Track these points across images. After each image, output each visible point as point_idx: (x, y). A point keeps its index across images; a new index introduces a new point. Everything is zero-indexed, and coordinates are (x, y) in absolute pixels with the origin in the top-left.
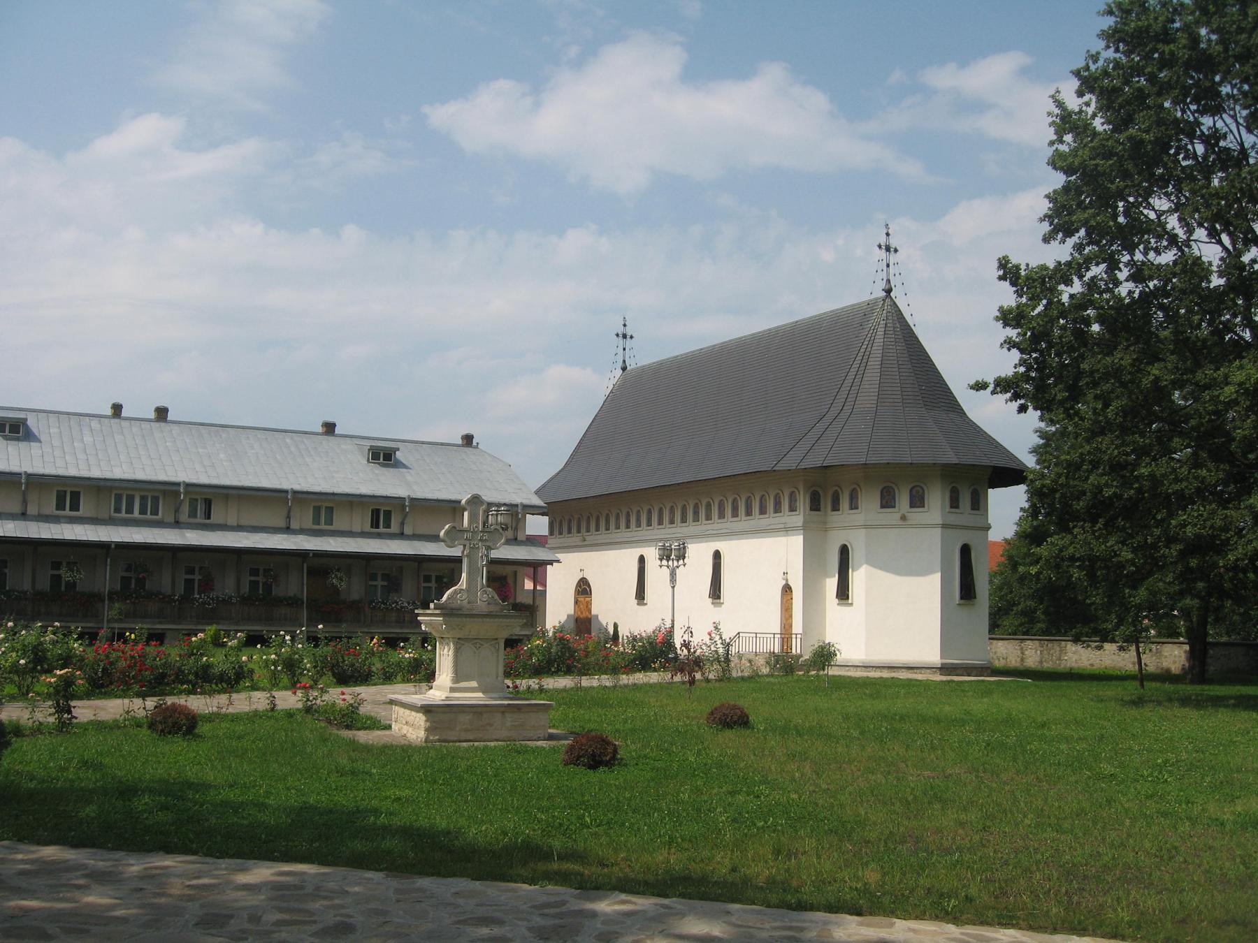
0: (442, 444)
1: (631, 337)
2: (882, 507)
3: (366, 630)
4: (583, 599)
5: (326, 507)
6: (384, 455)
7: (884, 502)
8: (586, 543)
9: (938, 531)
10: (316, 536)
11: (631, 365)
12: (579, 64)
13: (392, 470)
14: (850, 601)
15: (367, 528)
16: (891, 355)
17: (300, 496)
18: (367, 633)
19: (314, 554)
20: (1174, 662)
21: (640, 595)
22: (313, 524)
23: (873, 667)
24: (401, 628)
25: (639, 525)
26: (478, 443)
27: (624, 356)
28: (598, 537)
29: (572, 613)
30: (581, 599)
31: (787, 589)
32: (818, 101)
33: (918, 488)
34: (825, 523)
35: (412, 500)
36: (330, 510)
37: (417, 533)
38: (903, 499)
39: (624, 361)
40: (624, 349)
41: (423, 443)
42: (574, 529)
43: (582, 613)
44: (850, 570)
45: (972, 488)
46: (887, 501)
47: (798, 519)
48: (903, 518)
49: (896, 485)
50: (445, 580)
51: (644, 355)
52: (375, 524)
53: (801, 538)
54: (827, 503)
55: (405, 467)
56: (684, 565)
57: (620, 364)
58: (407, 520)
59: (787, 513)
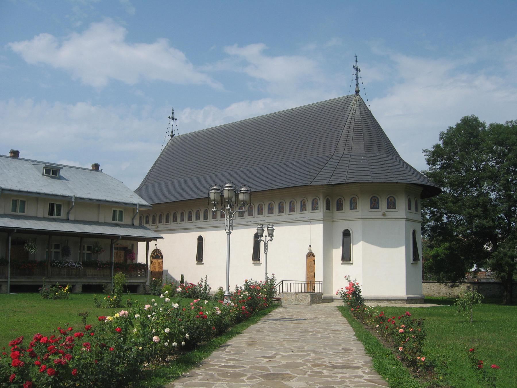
1: (176, 120)
2: (371, 208)
3: (48, 280)
4: (156, 261)
5: (21, 201)
6: (53, 171)
7: (372, 205)
8: (158, 229)
10: (16, 219)
11: (176, 135)
12: (80, 31)
13: (58, 180)
14: (351, 262)
15: (47, 215)
16: (366, 124)
17: (6, 192)
18: (49, 282)
19: (17, 230)
21: (199, 258)
22: (12, 211)
24: (71, 278)
26: (102, 170)
27: (172, 129)
28: (182, 225)
31: (311, 255)
32: (181, 55)
33: (392, 198)
34: (333, 218)
35: (77, 198)
36: (23, 203)
37: (77, 219)
38: (383, 204)
39: (172, 132)
40: (172, 126)
44: (351, 245)
45: (408, 197)
46: (374, 205)
47: (320, 214)
48: (384, 215)
51: (181, 131)
52: (51, 213)
53: (321, 226)
54: (334, 206)
56: (271, 241)
57: (170, 134)
58: (71, 212)
59: (299, 212)
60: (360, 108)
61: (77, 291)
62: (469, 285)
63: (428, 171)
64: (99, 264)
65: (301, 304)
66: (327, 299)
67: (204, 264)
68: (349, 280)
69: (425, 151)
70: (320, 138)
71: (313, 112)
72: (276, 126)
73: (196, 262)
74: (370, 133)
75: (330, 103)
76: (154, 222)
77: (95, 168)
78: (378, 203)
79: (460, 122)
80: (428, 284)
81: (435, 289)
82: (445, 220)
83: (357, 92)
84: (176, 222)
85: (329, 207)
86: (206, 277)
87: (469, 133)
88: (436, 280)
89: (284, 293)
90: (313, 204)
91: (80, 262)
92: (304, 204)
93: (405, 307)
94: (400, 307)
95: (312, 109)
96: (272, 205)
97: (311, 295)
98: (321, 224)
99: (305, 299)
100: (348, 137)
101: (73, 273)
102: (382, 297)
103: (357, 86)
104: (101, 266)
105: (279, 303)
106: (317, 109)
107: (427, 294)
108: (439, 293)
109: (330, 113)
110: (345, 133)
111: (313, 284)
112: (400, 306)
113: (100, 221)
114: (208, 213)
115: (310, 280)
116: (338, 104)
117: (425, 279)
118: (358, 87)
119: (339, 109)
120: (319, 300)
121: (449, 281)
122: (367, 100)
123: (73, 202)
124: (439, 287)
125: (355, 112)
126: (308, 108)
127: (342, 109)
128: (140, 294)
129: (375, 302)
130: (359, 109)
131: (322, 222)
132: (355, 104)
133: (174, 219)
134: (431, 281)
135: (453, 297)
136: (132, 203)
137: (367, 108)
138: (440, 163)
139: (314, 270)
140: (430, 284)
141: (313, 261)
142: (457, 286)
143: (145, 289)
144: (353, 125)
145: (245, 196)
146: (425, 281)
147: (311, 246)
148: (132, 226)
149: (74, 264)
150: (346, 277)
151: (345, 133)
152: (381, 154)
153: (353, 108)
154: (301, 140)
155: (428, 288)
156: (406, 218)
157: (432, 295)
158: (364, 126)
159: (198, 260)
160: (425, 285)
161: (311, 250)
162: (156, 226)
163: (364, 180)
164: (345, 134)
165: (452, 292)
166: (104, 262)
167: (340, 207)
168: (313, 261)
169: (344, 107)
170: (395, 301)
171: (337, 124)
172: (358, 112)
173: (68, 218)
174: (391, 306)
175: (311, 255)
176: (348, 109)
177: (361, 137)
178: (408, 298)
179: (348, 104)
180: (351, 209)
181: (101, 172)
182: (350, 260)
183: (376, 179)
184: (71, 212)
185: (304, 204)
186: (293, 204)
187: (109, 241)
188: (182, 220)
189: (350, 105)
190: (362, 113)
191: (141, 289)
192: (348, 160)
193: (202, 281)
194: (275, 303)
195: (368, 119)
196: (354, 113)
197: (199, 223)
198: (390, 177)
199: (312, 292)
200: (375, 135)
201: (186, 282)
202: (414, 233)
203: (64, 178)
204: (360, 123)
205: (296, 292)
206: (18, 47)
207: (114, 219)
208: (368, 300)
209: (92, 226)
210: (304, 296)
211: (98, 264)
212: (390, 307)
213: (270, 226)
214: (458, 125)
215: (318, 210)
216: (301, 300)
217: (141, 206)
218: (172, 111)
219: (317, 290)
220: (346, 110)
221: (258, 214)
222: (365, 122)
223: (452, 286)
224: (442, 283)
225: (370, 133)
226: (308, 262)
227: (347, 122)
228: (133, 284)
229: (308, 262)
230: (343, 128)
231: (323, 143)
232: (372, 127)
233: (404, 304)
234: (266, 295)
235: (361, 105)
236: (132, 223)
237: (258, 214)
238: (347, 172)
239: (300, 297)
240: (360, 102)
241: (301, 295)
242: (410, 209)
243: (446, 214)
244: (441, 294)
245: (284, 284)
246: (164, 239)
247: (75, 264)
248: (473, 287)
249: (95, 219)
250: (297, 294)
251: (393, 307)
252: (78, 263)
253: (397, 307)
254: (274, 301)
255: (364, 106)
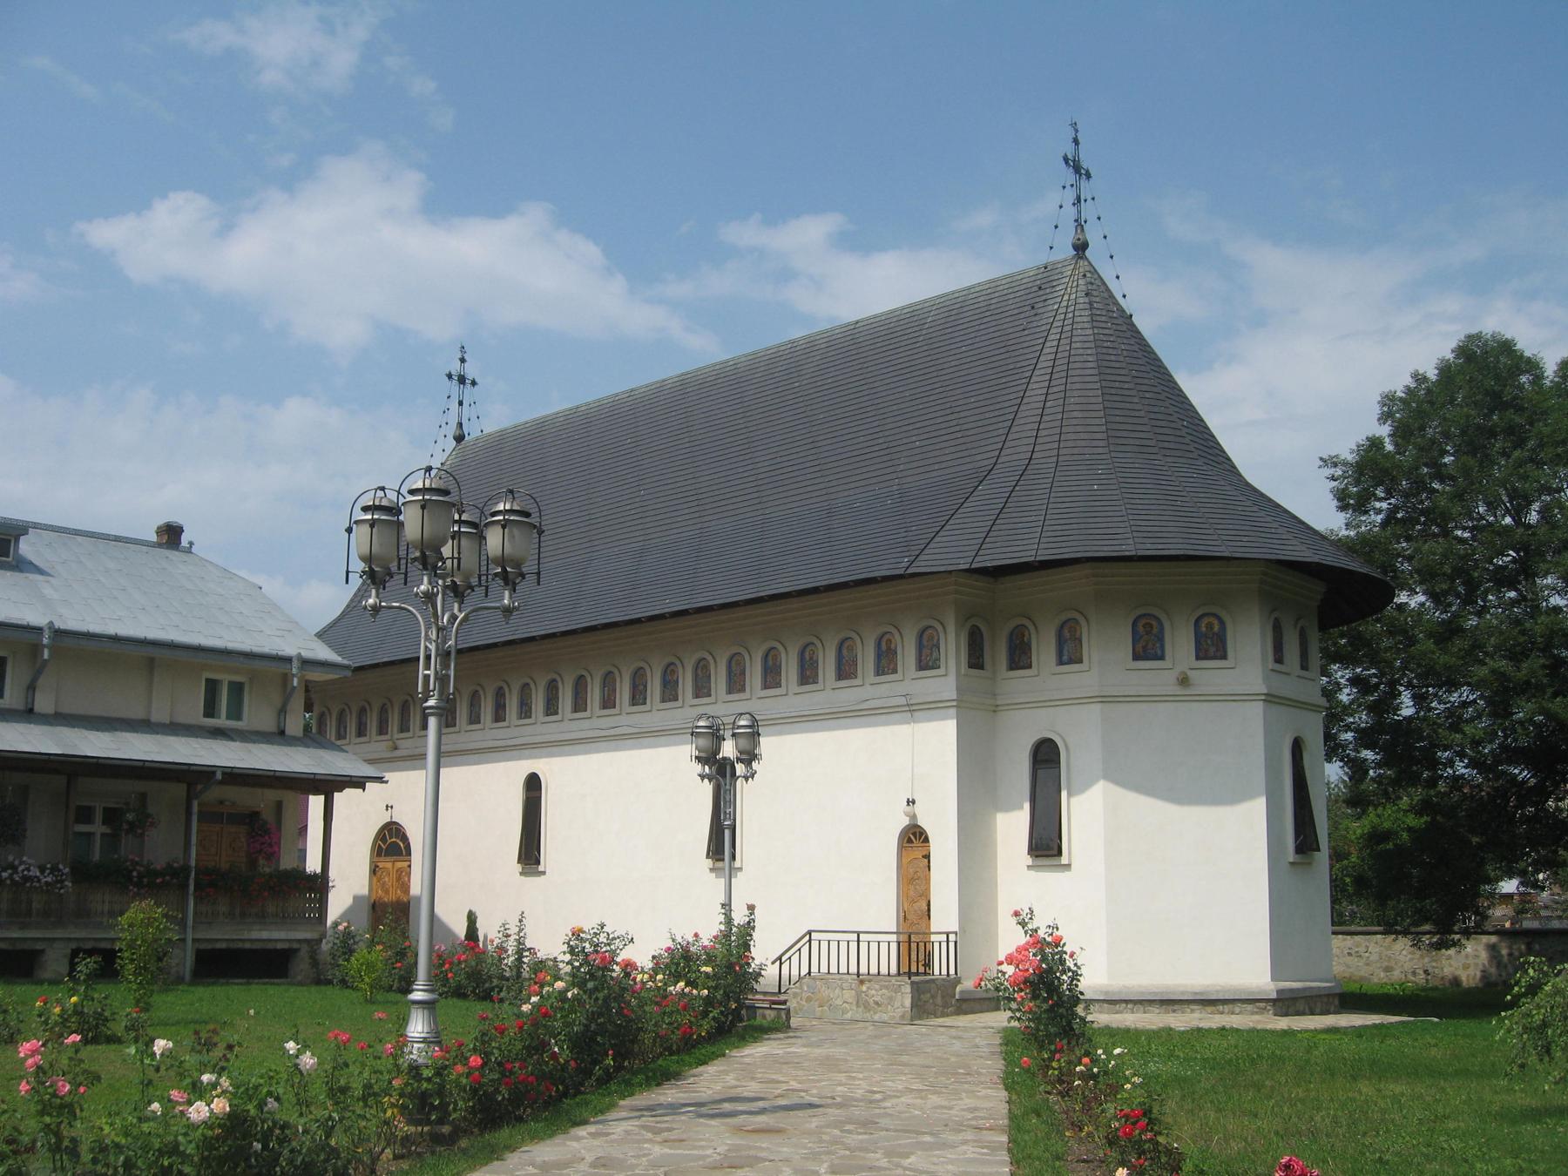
0: (117, 539)
2: (1136, 657)
4: (389, 865)
7: (1139, 647)
8: (397, 753)
9: (1256, 710)
11: (473, 431)
13: (9, 574)
14: (1064, 860)
16: (1113, 358)
20: (1466, 967)
21: (530, 853)
23: (1126, 1002)
24: (23, 927)
25: (525, 711)
26: (191, 544)
27: (460, 416)
29: (365, 891)
30: (386, 864)
31: (914, 837)
33: (1212, 619)
37: (66, 710)
38: (1180, 643)
39: (460, 425)
40: (461, 403)
41: (77, 533)
42: (372, 725)
43: (387, 892)
44: (1064, 794)
46: (1148, 647)
47: (944, 683)
48: (1184, 681)
49: (1087, 621)
50: (130, 817)
55: (40, 571)
57: (451, 430)
59: (871, 678)
60: (1090, 303)
61: (47, 975)
62: (1493, 939)
63: (1344, 533)
64: (135, 874)
65: (876, 1017)
66: (975, 1000)
67: (544, 873)
68: (1030, 926)
69: (1331, 462)
70: (948, 411)
71: (927, 326)
72: (797, 384)
73: (519, 868)
74: (1126, 386)
75: (984, 293)
76: (382, 730)
77: (166, 537)
78: (1161, 639)
79: (1450, 356)
80: (1349, 937)
81: (1374, 957)
82: (1407, 708)
83: (1081, 247)
84: (455, 725)
85: (982, 656)
86: (521, 921)
87: (1487, 393)
88: (1372, 924)
89: (814, 979)
90: (920, 647)
91: (61, 867)
92: (889, 648)
93: (1269, 1027)
94: (1253, 1031)
95: (921, 317)
96: (775, 658)
97: (913, 983)
98: (952, 718)
99: (891, 998)
100: (1048, 404)
101: (34, 905)
102: (1181, 989)
103: (1080, 224)
104: (145, 880)
105: (779, 1016)
106: (938, 317)
107: (1347, 975)
108: (1388, 969)
109: (982, 327)
110: (1037, 388)
111: (921, 945)
112: (1251, 1025)
113: (155, 718)
114: (557, 689)
115: (914, 929)
116: (1012, 296)
117: (1340, 923)
118: (1083, 230)
119: (1016, 312)
120: (945, 1005)
121: (1427, 927)
122: (1099, 218)
123: (44, 646)
124: (1389, 948)
125: (1071, 315)
126: (908, 316)
127: (1026, 308)
128: (301, 984)
129: (1155, 1009)
130: (1087, 306)
131: (953, 711)
132: (1074, 290)
133: (450, 718)
134: (1353, 928)
135: (1437, 983)
136: (274, 652)
137: (1116, 303)
138: (1384, 505)
139: (928, 889)
140: (1357, 938)
141: (924, 857)
142: (1455, 944)
143: (315, 962)
144: (1066, 361)
145: (512, 537)
146: (1337, 928)
147: (914, 802)
148: (279, 736)
149: (35, 872)
150: (1016, 914)
151: (1037, 388)
152: (1169, 459)
153: (1064, 304)
154: (883, 422)
155: (1350, 954)
156: (1265, 692)
157: (1362, 978)
158: (1105, 363)
159: (525, 858)
160: (1340, 943)
161: (914, 817)
162: (391, 743)
163: (1105, 548)
164: (1036, 392)
165: (1434, 964)
166: (159, 865)
167: (1019, 657)
168: (924, 857)
169: (1033, 301)
170: (1231, 1006)
171: (1010, 361)
172: (1084, 317)
173: (30, 706)
174: (1214, 1026)
175: (914, 834)
176: (1050, 308)
177: (1093, 400)
178: (1279, 992)
179: (1048, 291)
180: (1061, 662)
181: (189, 551)
182: (1060, 853)
183: (1149, 546)
184: (41, 682)
185: (889, 648)
186: (851, 649)
187: (179, 790)
188: (474, 719)
189: (1056, 294)
190: (1098, 318)
191: (302, 966)
192: (1045, 486)
193: (508, 936)
194: (764, 1017)
195: (1119, 340)
196: (1069, 328)
197: (529, 730)
198: (1204, 537)
199: (917, 974)
200: (1147, 395)
201: (486, 937)
202: (1297, 747)
203: (35, 566)
204: (1089, 352)
205: (858, 974)
206: (106, 234)
207: (210, 710)
208: (1131, 1001)
209: (119, 734)
210: (887, 987)
211: (131, 871)
212: (1210, 1030)
213: (742, 723)
214: (1445, 370)
215: (939, 667)
216: (877, 1003)
217: (306, 663)
218: (459, 356)
219: (941, 967)
220: (1040, 311)
221: (730, 692)
222: (1111, 351)
223: (1439, 946)
224: (1405, 933)
225: (1126, 386)
226: (905, 861)
227: (1045, 351)
228: (270, 946)
229: (905, 861)
230: (1029, 374)
231: (958, 428)
232: (1135, 367)
233: (1266, 1015)
234: (706, 992)
235: (1095, 293)
236: (279, 727)
237: (730, 692)
238: (1041, 523)
239: (875, 993)
240: (1092, 283)
241: (877, 987)
242: (1279, 659)
243: (1410, 686)
244: (1397, 975)
245: (815, 945)
246: (387, 782)
247: (42, 872)
248: (1510, 948)
249: (137, 713)
250: (862, 982)
251: (1223, 1028)
252: (54, 869)
253: (1237, 1030)
254: (761, 1011)
255: (1106, 295)
